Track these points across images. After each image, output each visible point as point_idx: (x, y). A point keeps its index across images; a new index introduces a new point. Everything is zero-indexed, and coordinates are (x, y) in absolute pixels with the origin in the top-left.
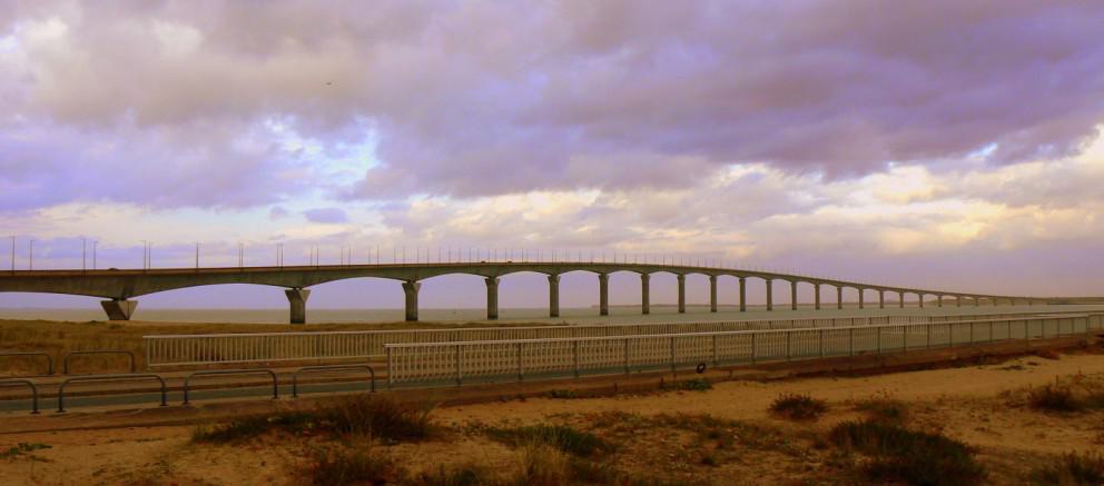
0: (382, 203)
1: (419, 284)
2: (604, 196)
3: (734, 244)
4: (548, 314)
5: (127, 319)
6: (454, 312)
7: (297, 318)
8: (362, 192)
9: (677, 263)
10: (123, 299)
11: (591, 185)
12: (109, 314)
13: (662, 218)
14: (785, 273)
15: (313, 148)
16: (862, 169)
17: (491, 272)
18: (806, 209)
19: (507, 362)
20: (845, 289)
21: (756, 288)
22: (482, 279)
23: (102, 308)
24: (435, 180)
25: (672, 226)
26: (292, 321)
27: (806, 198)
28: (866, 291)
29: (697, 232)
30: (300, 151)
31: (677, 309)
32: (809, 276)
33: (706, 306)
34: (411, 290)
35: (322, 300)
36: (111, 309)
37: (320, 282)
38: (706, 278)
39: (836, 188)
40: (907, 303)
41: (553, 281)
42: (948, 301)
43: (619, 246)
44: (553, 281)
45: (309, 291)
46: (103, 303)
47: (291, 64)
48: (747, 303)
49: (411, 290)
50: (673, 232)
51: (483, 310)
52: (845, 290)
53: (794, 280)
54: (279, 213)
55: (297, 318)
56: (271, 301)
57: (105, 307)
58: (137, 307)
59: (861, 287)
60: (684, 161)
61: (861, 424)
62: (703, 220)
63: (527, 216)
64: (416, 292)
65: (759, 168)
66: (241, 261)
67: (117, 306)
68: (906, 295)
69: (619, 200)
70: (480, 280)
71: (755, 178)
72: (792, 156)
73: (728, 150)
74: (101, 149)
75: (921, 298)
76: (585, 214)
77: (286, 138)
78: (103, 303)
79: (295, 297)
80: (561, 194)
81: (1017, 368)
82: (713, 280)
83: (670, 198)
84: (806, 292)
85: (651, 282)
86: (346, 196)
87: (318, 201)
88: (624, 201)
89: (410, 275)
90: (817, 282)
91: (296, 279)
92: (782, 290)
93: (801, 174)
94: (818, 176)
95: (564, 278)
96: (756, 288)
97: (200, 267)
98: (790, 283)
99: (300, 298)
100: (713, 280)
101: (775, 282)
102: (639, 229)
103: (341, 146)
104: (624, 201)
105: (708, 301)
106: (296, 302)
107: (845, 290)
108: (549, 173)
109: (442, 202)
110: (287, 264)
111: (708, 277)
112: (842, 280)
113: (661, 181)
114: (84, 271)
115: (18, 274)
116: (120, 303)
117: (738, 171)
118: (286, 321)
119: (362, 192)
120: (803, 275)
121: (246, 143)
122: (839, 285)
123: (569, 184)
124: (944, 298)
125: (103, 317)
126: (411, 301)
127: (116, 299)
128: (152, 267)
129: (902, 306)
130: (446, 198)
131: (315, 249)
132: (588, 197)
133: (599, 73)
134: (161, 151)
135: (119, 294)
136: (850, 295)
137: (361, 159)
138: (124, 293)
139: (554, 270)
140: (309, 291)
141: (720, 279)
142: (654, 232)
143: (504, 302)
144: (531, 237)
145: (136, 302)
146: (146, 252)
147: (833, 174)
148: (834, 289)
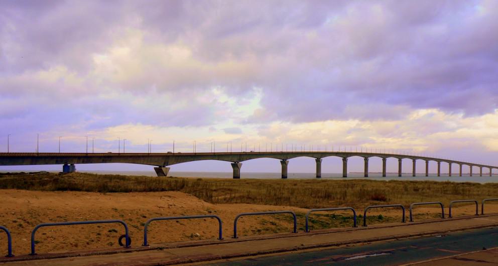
0: (259, 125)
1: (288, 161)
2: (360, 123)
3: (418, 146)
4: (342, 176)
5: (166, 176)
6: (294, 174)
7: (236, 175)
8: (251, 121)
9: (383, 152)
10: (164, 167)
11: (355, 118)
12: (157, 173)
13: (385, 133)
14: (446, 159)
15: (232, 101)
16: (482, 111)
17: (319, 156)
18: (453, 130)
21: (433, 165)
22: (279, 161)
23: (154, 170)
24: (284, 115)
25: (389, 137)
26: (234, 177)
27: (453, 125)
28: (483, 168)
29: (400, 140)
30: (226, 103)
31: (398, 175)
33: (380, 173)
34: (284, 164)
35: (248, 168)
36: (159, 171)
37: (247, 160)
38: (411, 161)
39: (468, 120)
40: (493, 174)
41: (345, 160)
43: (363, 145)
44: (345, 160)
45: (242, 164)
46: (155, 168)
47: (230, 65)
48: (429, 173)
49: (284, 164)
50: (390, 140)
52: (484, 168)
53: (450, 162)
54: (212, 130)
55: (236, 175)
56: (224, 169)
57: (155, 170)
58: (170, 171)
59: (481, 166)
60: (399, 108)
62: (404, 134)
63: (323, 132)
64: (286, 165)
65: (434, 111)
66: (333, 150)
67: (162, 169)
68: (493, 169)
69: (367, 125)
71: (431, 115)
72: (450, 106)
73: (419, 103)
74: (139, 102)
76: (349, 132)
77: (218, 95)
78: (155, 168)
79: (235, 166)
80: (339, 122)
81: (270, 211)
82: (414, 162)
83: (390, 124)
84: (455, 168)
85: (402, 162)
86: (244, 123)
87: (230, 124)
88: (369, 125)
89: (284, 157)
90: (461, 164)
91: (237, 158)
92: (445, 167)
93: (453, 114)
94: (461, 115)
95: (350, 159)
96: (433, 165)
97: (175, 152)
98: (448, 164)
99: (238, 167)
100: (400, 161)
101: (453, 165)
102: (375, 138)
103: (244, 100)
104: (369, 125)
106: (236, 169)
108: (336, 112)
109: (286, 125)
110: (233, 151)
111: (425, 161)
112: (462, 161)
113: (387, 116)
114: (119, 154)
115: (122, 155)
116: (163, 168)
117: (423, 112)
118: (232, 177)
119: (251, 121)
121: (202, 98)
122: (471, 165)
123: (345, 117)
125: (155, 175)
126: (284, 169)
127: (160, 167)
128: (152, 152)
130: (288, 123)
131: (229, 145)
132: (352, 123)
133: (368, 68)
134: (167, 103)
135: (162, 164)
136: (476, 170)
137: (254, 103)
138: (165, 163)
139: (345, 156)
140: (242, 164)
141: (388, 160)
142: (381, 139)
143: (324, 171)
144: (324, 141)
145: (169, 168)
146: (149, 146)
147: (468, 114)
148: (469, 167)
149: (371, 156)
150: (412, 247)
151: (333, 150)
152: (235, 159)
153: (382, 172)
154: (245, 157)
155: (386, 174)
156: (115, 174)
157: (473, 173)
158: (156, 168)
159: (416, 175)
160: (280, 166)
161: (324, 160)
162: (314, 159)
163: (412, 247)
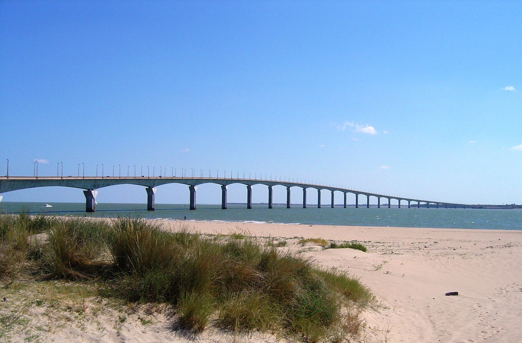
19: (324, 303)
20: (370, 197)
21: (326, 195)
32: (353, 190)
33: (284, 204)
42: (414, 206)
51: (188, 205)
53: (345, 191)
57: (87, 212)
61: (182, 317)
66: (384, 194)
70: (187, 187)
75: (409, 203)
90: (357, 193)
105: (246, 202)
107: (371, 197)
120: (350, 189)
124: (421, 203)
129: (368, 207)
149: (421, 202)
150: (374, 323)
151: (250, 178)
152: (369, 195)
153: (355, 204)
154: (360, 193)
155: (321, 206)
156: (205, 221)
157: (401, 204)
158: (147, 188)
159: (321, 206)
160: (408, 203)
161: (391, 200)
162: (220, 186)
163: (374, 323)
